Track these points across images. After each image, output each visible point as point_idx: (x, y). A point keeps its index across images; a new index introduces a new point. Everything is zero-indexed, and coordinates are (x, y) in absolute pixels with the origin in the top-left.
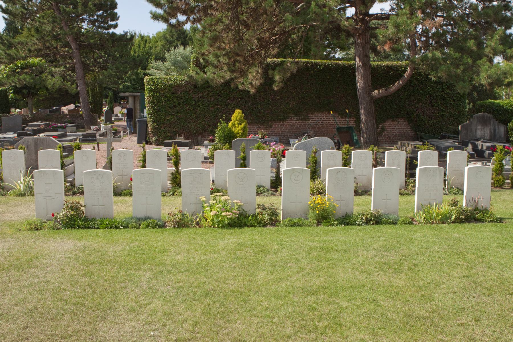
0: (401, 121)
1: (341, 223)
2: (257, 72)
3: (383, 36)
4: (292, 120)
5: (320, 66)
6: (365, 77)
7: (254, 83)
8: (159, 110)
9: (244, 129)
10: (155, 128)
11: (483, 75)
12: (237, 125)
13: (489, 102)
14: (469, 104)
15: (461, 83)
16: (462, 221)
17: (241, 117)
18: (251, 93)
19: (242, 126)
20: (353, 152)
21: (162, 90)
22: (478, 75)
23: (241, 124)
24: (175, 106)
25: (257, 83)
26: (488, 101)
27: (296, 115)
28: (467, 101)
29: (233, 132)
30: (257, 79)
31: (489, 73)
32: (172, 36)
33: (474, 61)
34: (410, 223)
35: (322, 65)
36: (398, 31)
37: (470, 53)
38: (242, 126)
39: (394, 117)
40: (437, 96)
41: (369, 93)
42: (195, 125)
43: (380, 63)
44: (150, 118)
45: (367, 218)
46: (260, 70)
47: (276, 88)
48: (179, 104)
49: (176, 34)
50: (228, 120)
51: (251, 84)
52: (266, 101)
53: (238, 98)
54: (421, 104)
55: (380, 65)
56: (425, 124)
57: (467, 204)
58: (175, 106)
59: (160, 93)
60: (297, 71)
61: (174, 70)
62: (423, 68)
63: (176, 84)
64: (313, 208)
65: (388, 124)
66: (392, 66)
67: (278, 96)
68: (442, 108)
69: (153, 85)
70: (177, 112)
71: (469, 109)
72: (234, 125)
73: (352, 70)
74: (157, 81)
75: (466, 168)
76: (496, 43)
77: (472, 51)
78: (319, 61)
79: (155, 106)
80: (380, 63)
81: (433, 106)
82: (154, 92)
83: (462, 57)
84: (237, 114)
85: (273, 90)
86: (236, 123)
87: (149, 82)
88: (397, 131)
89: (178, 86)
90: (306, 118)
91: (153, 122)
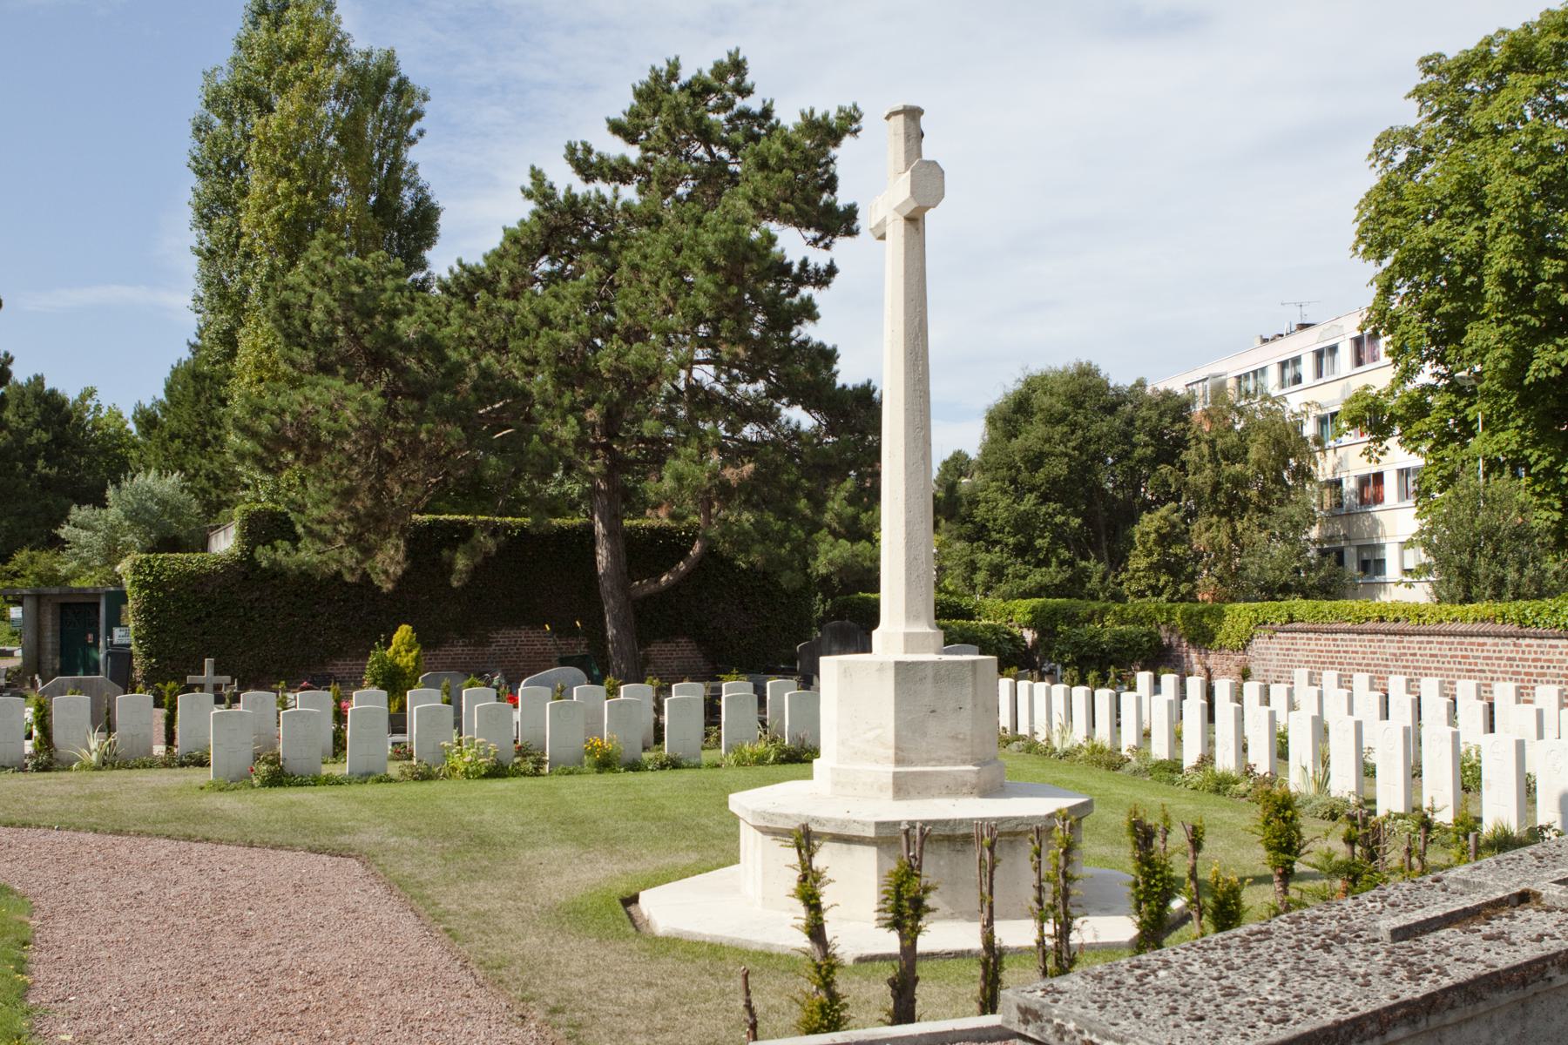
0: (683, 641)
1: (627, 770)
2: (397, 548)
3: (657, 494)
4: (453, 646)
5: (513, 531)
6: (613, 554)
7: (391, 571)
8: (161, 630)
9: (417, 659)
10: (153, 669)
11: (822, 559)
12: (403, 653)
13: (859, 598)
14: (824, 602)
15: (788, 572)
16: (783, 762)
17: (411, 638)
18: (385, 590)
19: (414, 653)
20: (622, 688)
21: (170, 584)
22: (815, 558)
23: (411, 651)
24: (198, 620)
25: (396, 570)
26: (856, 596)
27: (463, 636)
28: (820, 596)
29: (397, 666)
30: (398, 563)
31: (830, 555)
32: (23, 418)
33: (810, 533)
34: (718, 766)
35: (517, 527)
36: (681, 487)
37: (802, 520)
38: (414, 653)
39: (669, 635)
40: (753, 587)
41: (624, 588)
42: (244, 662)
43: (635, 522)
44: (140, 646)
45: (661, 763)
46: (402, 543)
47: (455, 584)
48: (209, 615)
49: (37, 413)
50: (388, 644)
51: (386, 572)
52: (399, 605)
53: (338, 601)
54: (722, 605)
55: (636, 526)
56: (733, 648)
57: (790, 742)
58: (198, 620)
59: (165, 591)
60: (497, 553)
61: (130, 530)
62: (725, 547)
63: (202, 571)
64: (590, 753)
65: (655, 649)
66: (660, 528)
67: (424, 595)
68: (764, 612)
69: (149, 575)
70: (204, 633)
71: (824, 612)
72: (397, 652)
73: (585, 537)
74: (160, 565)
75: (787, 695)
76: (840, 505)
77: (805, 517)
78: (510, 519)
79: (153, 619)
80: (635, 522)
81: (746, 609)
82: (150, 589)
83: (788, 528)
84: (403, 633)
85: (449, 585)
86: (402, 648)
87: (139, 566)
88: (675, 663)
89: (207, 575)
90: (484, 642)
91: (148, 655)
